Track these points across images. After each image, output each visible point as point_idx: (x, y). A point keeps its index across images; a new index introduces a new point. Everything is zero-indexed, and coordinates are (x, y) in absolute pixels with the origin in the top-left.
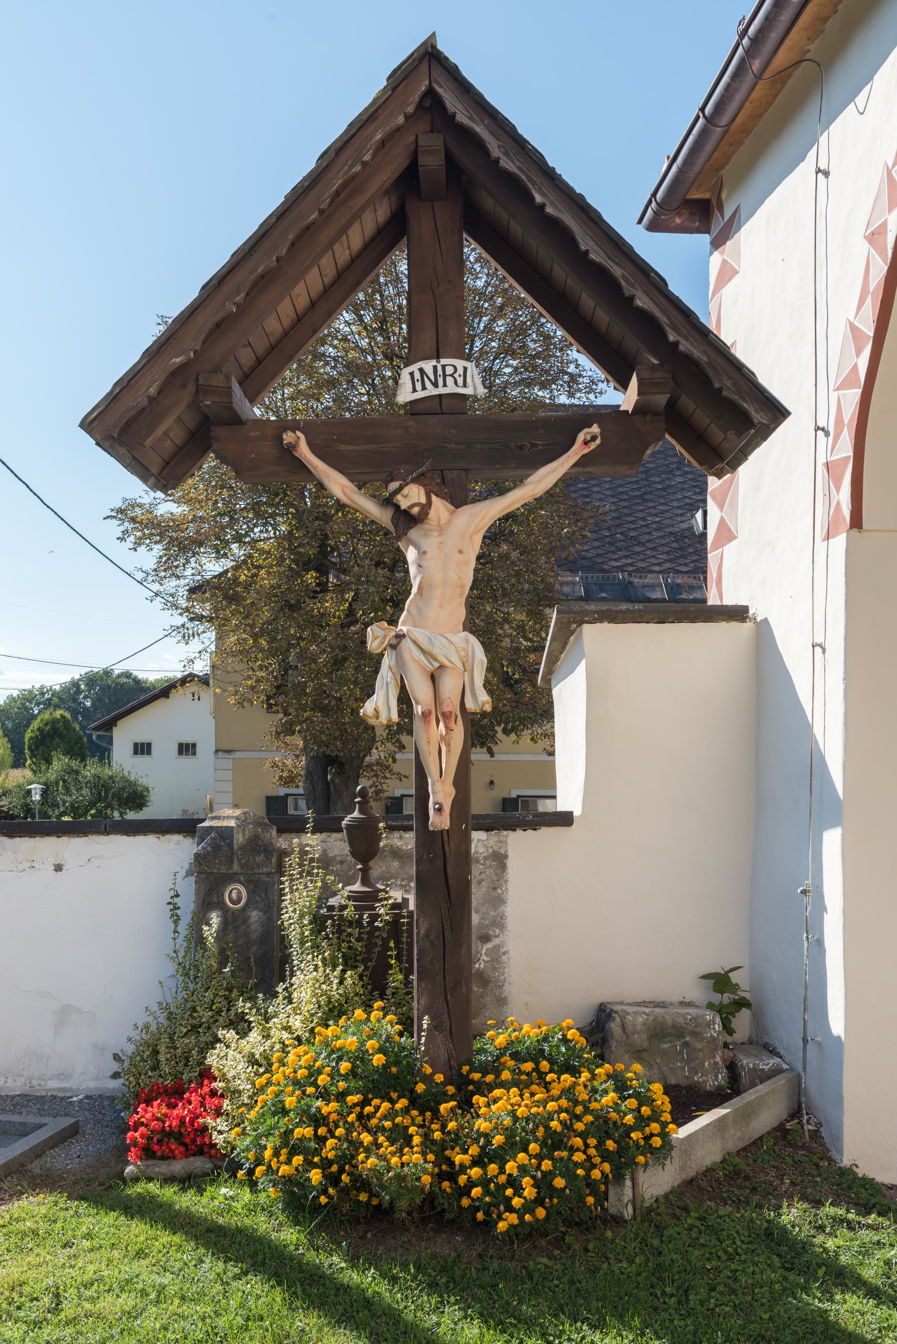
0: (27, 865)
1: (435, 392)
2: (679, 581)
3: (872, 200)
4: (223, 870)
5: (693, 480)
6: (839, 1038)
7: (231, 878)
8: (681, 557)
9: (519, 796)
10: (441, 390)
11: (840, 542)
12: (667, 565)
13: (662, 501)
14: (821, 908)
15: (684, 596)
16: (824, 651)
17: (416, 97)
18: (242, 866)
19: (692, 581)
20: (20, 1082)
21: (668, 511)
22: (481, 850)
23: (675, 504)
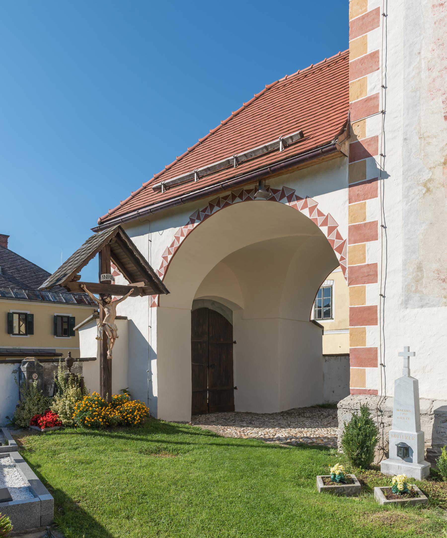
1: (107, 280)
4: (33, 370)
6: (156, 397)
7: (34, 372)
10: (108, 280)
14: (151, 374)
16: (151, 327)
17: (116, 233)
18: (37, 369)
22: (77, 366)
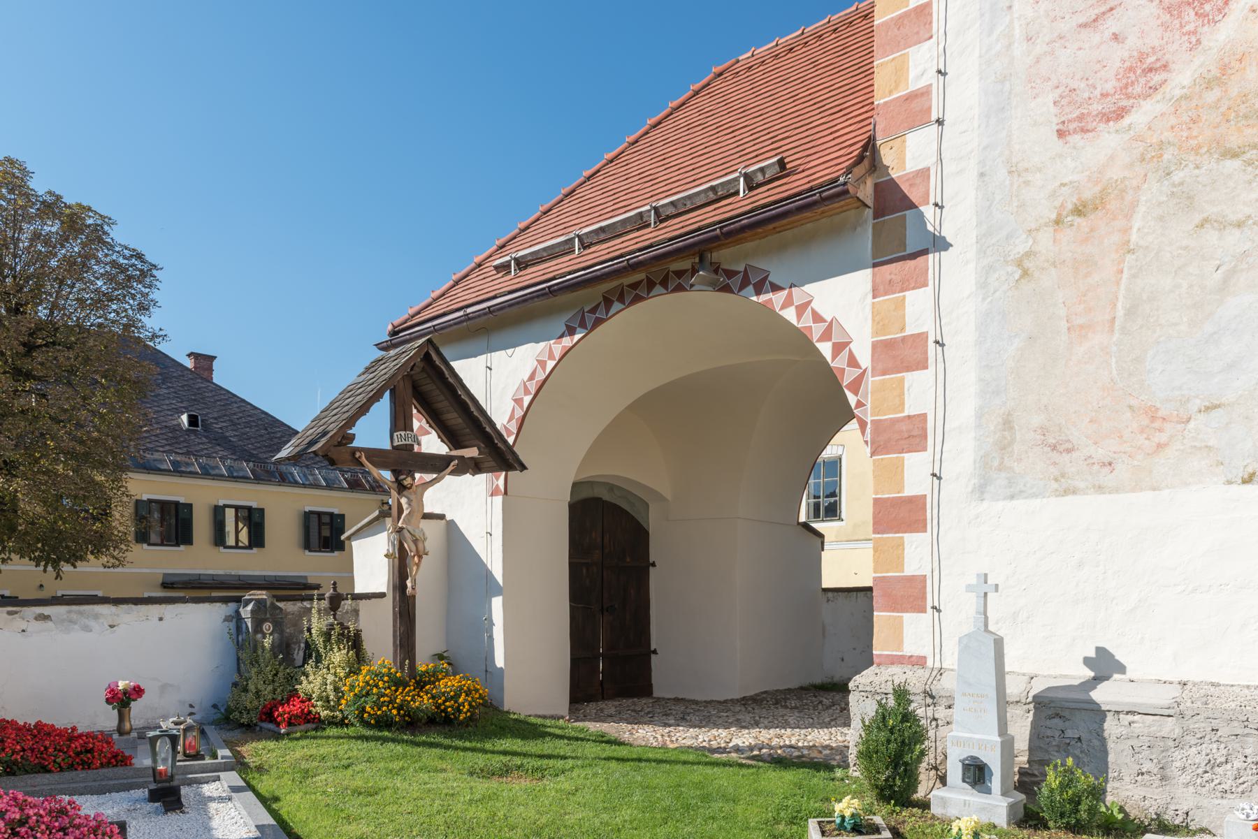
0: (145, 618)
2: (178, 459)
3: (516, 388)
5: (175, 392)
7: (266, 620)
8: (176, 443)
9: (63, 595)
10: (407, 443)
11: (499, 500)
12: (167, 448)
13: (156, 404)
15: (183, 469)
16: (491, 535)
18: (271, 615)
19: (187, 460)
20: (142, 721)
21: (161, 411)
23: (165, 407)
